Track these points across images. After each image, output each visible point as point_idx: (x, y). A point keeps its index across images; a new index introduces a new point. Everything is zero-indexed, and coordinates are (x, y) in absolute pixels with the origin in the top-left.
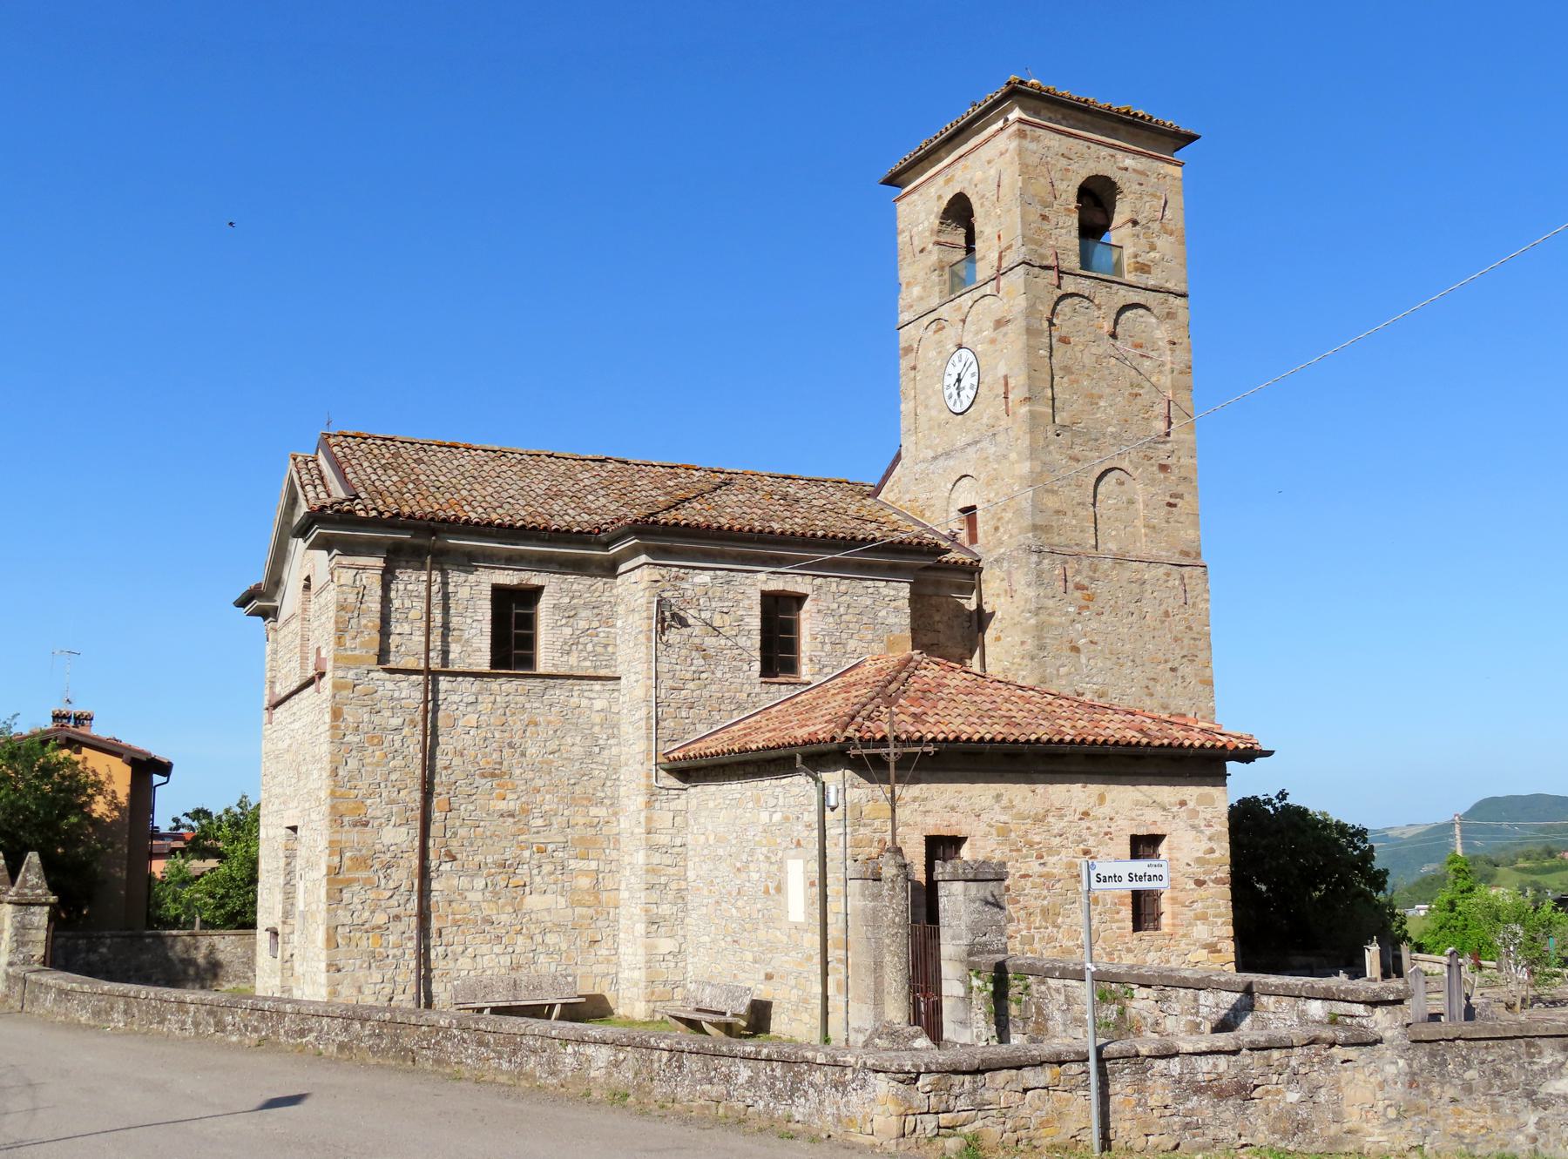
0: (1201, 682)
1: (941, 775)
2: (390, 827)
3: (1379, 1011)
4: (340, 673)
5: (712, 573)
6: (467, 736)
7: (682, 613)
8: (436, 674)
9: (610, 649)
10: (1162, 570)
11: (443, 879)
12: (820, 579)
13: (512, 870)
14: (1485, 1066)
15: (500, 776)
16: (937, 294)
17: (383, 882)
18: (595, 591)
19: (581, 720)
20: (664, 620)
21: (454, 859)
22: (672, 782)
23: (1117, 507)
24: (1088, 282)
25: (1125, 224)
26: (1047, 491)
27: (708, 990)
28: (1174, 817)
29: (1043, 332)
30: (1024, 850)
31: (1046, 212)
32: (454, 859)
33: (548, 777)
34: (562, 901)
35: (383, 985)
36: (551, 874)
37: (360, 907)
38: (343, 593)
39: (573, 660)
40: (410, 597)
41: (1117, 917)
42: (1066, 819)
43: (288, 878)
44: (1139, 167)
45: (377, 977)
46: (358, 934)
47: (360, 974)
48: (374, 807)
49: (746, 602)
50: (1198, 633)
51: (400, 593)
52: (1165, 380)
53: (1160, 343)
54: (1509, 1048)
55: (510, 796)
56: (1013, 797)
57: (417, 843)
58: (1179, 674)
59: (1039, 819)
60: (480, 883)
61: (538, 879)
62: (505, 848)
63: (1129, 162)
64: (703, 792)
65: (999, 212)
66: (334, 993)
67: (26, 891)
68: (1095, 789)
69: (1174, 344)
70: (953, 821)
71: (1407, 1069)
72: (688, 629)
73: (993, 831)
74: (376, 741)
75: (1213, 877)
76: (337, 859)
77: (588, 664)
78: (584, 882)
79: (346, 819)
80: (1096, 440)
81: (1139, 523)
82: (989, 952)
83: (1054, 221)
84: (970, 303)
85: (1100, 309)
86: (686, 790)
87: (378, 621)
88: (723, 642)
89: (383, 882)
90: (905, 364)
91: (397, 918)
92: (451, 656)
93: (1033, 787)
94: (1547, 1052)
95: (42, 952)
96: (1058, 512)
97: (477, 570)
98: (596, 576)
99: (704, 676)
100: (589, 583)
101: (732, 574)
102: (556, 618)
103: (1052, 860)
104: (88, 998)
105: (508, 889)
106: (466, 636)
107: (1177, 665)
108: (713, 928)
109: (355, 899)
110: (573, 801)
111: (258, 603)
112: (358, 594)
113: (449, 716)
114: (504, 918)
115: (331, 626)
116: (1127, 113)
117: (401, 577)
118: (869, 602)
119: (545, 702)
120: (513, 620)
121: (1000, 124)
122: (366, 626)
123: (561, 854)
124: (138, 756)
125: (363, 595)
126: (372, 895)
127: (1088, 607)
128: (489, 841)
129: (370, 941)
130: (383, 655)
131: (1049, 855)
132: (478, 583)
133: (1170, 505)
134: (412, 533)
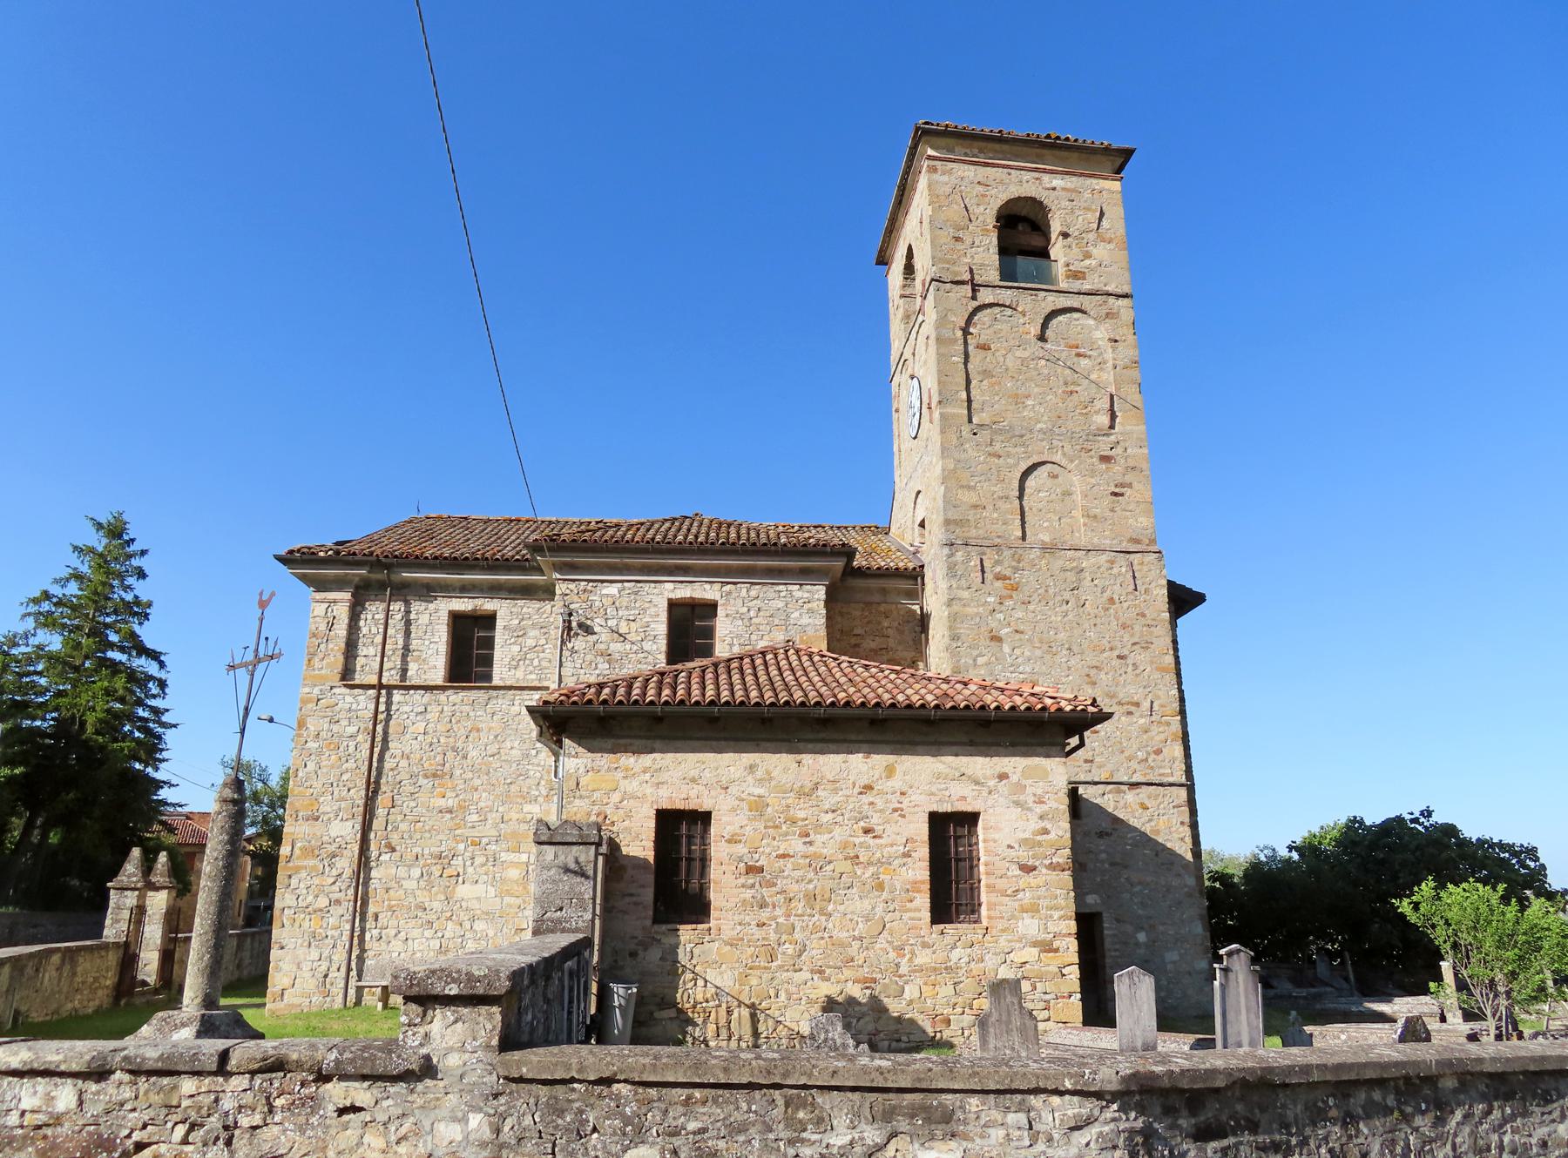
0: (1158, 669)
1: (679, 744)
2: (336, 821)
3: (440, 1019)
5: (620, 585)
6: (414, 742)
7: (589, 622)
8: (390, 688)
10: (1104, 557)
11: (381, 869)
12: (729, 586)
13: (447, 861)
14: (677, 1141)
19: (520, 726)
20: (570, 629)
21: (394, 850)
23: (1050, 499)
24: (1009, 292)
26: (962, 487)
28: (990, 793)
29: (956, 340)
30: (784, 827)
31: (960, 234)
32: (394, 850)
33: (486, 777)
34: (492, 893)
35: (320, 963)
36: (483, 865)
39: (519, 674)
41: (909, 905)
42: (840, 793)
44: (1069, 185)
45: (315, 955)
50: (1154, 620)
51: (368, 622)
52: (1108, 377)
53: (1100, 343)
54: (744, 1107)
56: (771, 769)
58: (1130, 661)
59: (803, 794)
60: (416, 872)
61: (470, 870)
62: (441, 841)
63: (1057, 182)
68: (880, 760)
69: (1116, 341)
70: (693, 794)
71: (487, 1134)
72: (594, 636)
73: (744, 805)
74: (332, 746)
75: (1047, 862)
78: (514, 874)
79: (300, 814)
80: (1022, 436)
81: (1077, 513)
82: (563, 931)
83: (968, 241)
85: (1024, 315)
87: (343, 645)
89: (327, 869)
91: (338, 902)
92: (409, 673)
93: (799, 757)
94: (841, 1121)
96: (975, 507)
98: (544, 601)
100: (538, 606)
101: (639, 585)
103: (819, 839)
107: (1125, 652)
110: (506, 799)
113: (400, 725)
114: (436, 905)
116: (1048, 136)
118: (781, 605)
122: (332, 650)
123: (494, 847)
125: (333, 624)
127: (1011, 597)
128: (427, 835)
130: (347, 673)
132: (437, 611)
133: (1115, 494)
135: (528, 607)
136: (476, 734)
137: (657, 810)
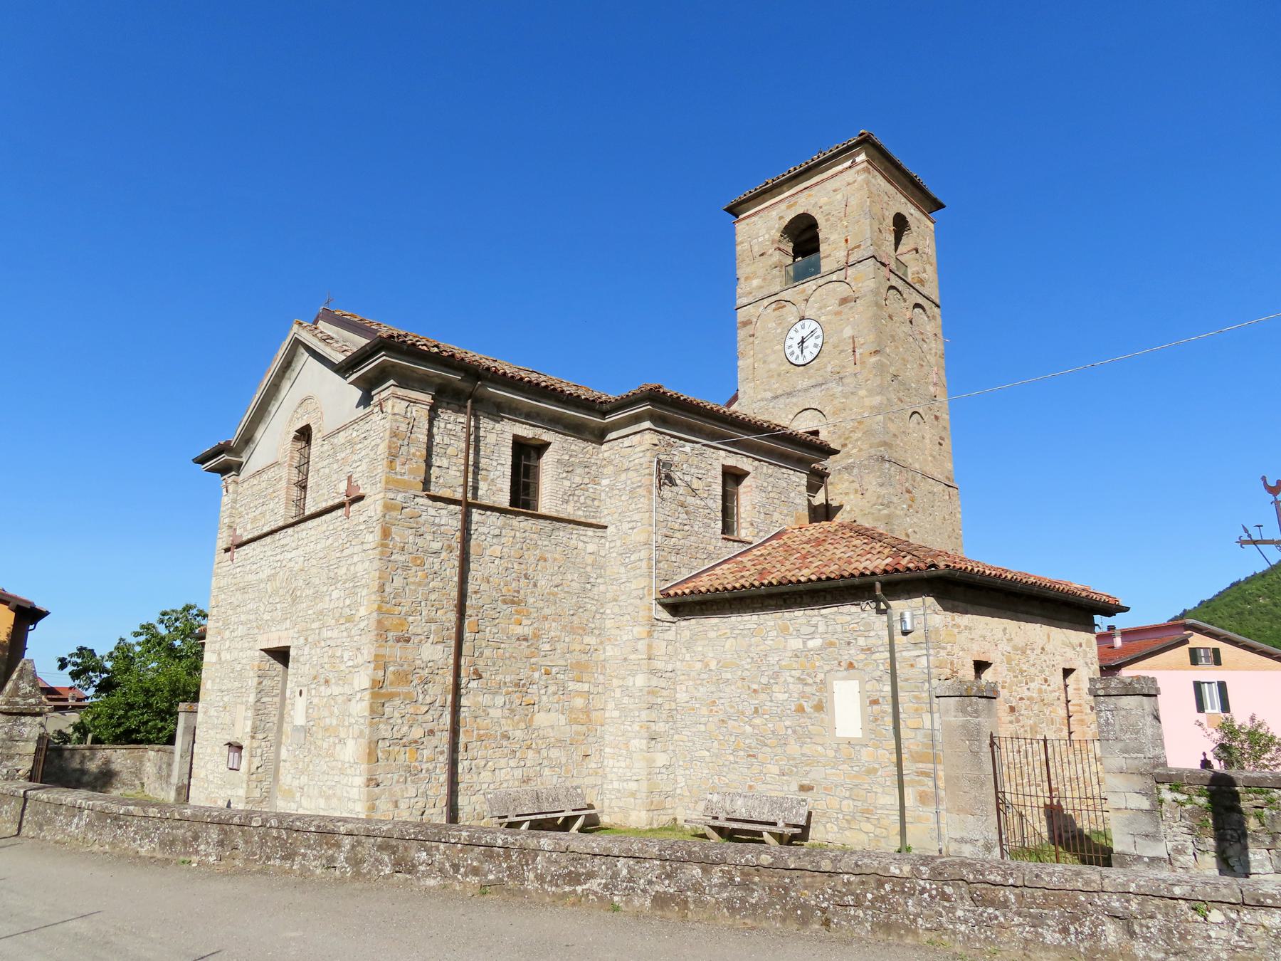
2: (428, 644)
4: (391, 495)
6: (492, 565)
9: (596, 503)
11: (470, 696)
15: (518, 603)
16: (778, 283)
17: (421, 697)
18: (587, 453)
22: (665, 615)
25: (909, 251)
27: (740, 802)
34: (563, 720)
35: (416, 800)
36: (555, 694)
37: (400, 721)
38: (396, 421)
43: (259, 696)
44: (917, 215)
45: (411, 791)
46: (397, 748)
47: (397, 788)
48: (415, 624)
49: (713, 472)
51: (441, 430)
55: (525, 622)
57: (451, 661)
60: (500, 700)
61: (544, 698)
64: (697, 623)
65: (846, 224)
66: (373, 808)
67: (18, 699)
74: (419, 562)
76: (381, 673)
77: (581, 513)
84: (814, 288)
86: (674, 623)
88: (698, 502)
89: (421, 697)
90: (742, 333)
92: (480, 492)
95: (29, 766)
97: (502, 421)
99: (686, 528)
102: (559, 471)
104: (155, 824)
105: (522, 707)
106: (492, 476)
108: (716, 743)
109: (395, 713)
110: (573, 631)
111: (226, 457)
112: (409, 424)
114: (518, 733)
115: (383, 448)
117: (442, 415)
118: (785, 485)
119: (552, 542)
120: (522, 470)
121: (849, 163)
122: (414, 454)
123: (562, 676)
124: (21, 604)
126: (410, 709)
128: (507, 662)
129: (407, 755)
130: (426, 483)
131: (1031, 682)
132: (503, 432)
134: (463, 375)
135: (575, 445)
136: (544, 564)
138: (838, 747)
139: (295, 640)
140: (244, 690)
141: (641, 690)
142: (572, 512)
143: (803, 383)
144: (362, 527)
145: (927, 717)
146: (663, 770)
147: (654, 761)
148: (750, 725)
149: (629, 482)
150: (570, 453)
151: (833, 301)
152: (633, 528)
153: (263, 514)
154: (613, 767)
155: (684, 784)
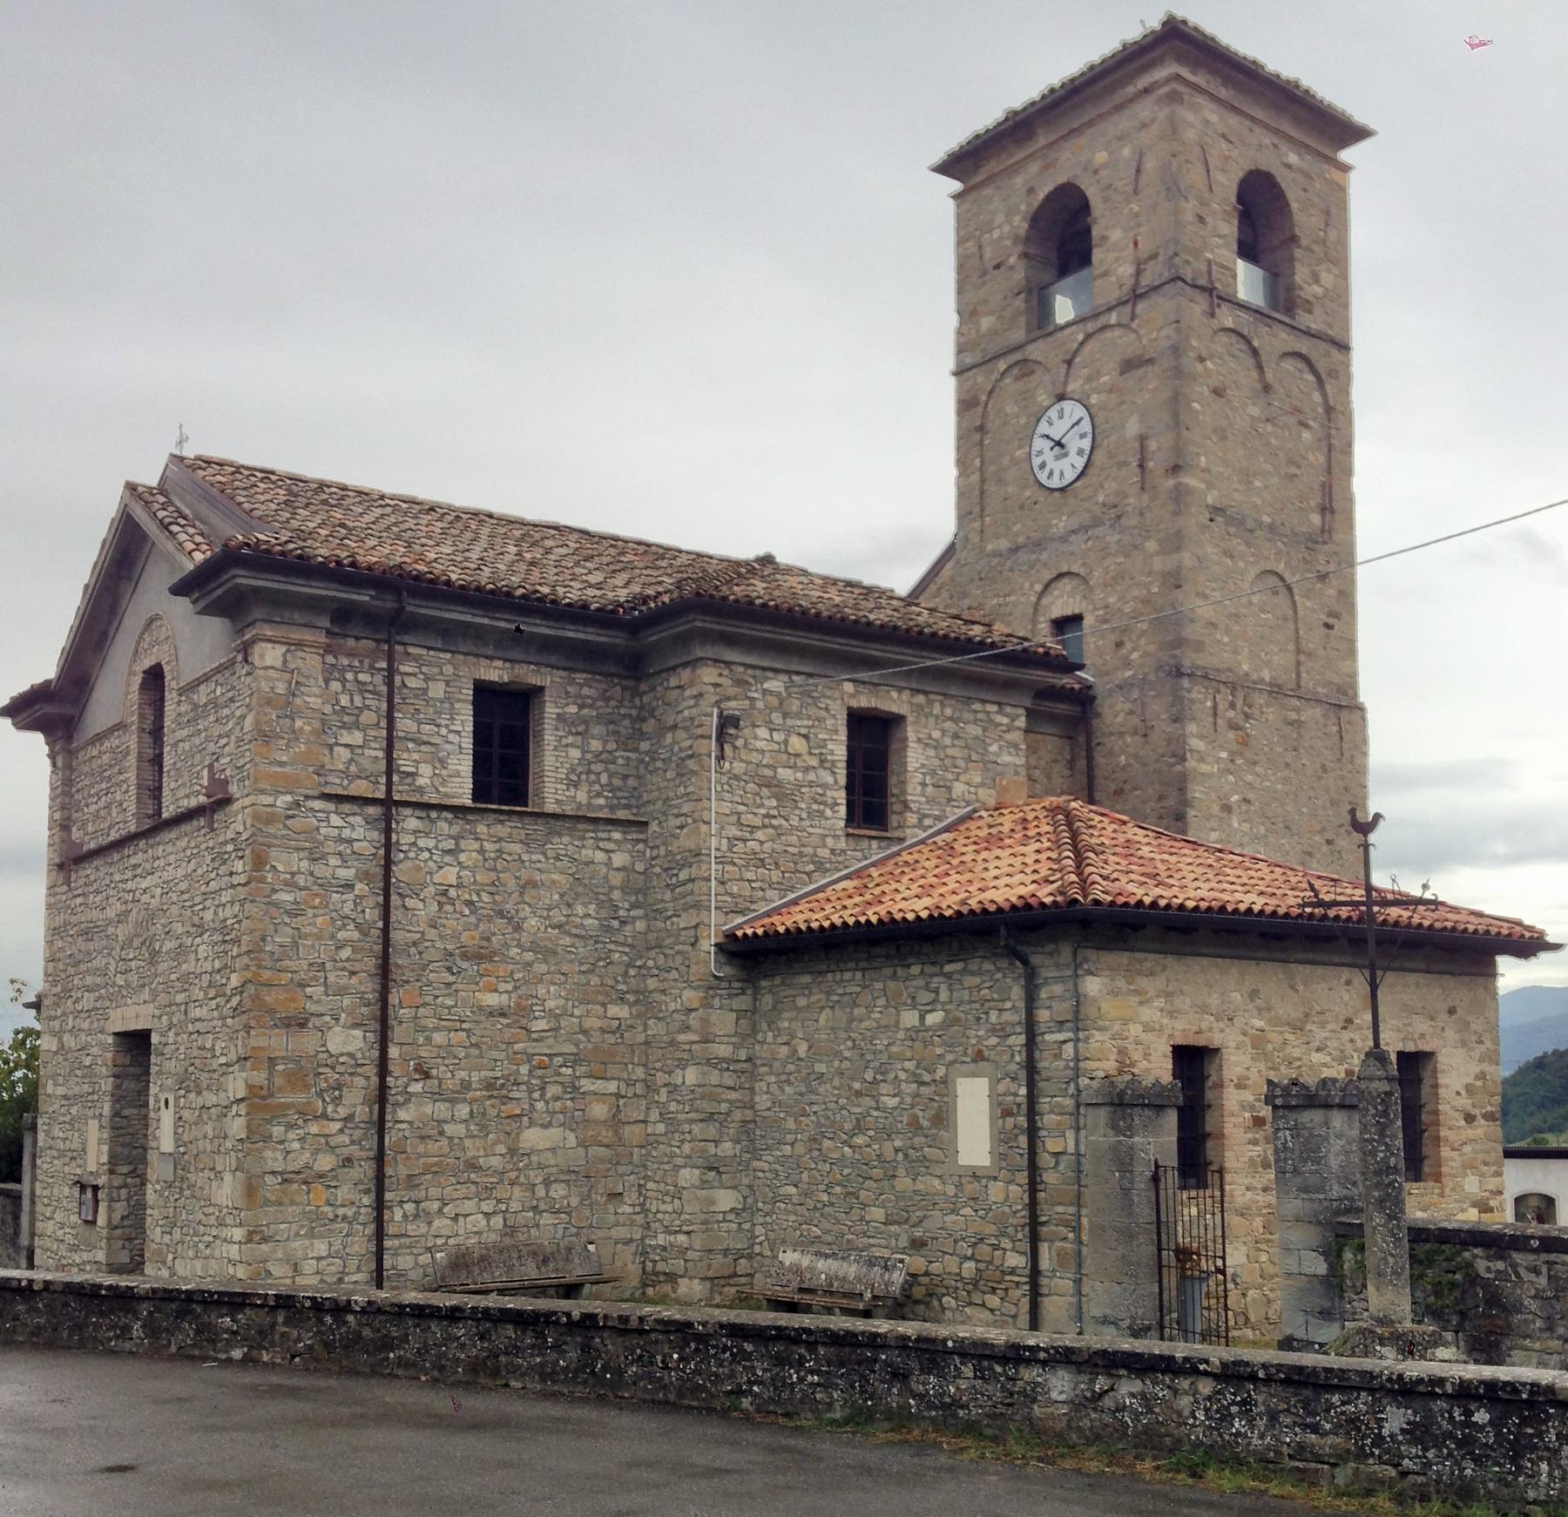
21: (427, 1076)
32: (427, 1076)
34: (572, 1140)
39: (582, 796)
40: (361, 692)
44: (1304, 165)
60: (463, 1111)
61: (540, 1105)
65: (1137, 209)
78: (599, 1110)
84: (1080, 337)
137: (1173, 1046)
138: (960, 1182)
139: (156, 1020)
140: (96, 1097)
141: (692, 1091)
142: (585, 801)
143: (1061, 524)
144: (230, 848)
145: (1070, 1135)
146: (731, 1217)
147: (714, 1203)
148: (850, 1147)
149: (676, 749)
150: (579, 702)
151: (1111, 365)
152: (681, 827)
153: (108, 807)
154: (658, 1212)
155: (762, 1238)
